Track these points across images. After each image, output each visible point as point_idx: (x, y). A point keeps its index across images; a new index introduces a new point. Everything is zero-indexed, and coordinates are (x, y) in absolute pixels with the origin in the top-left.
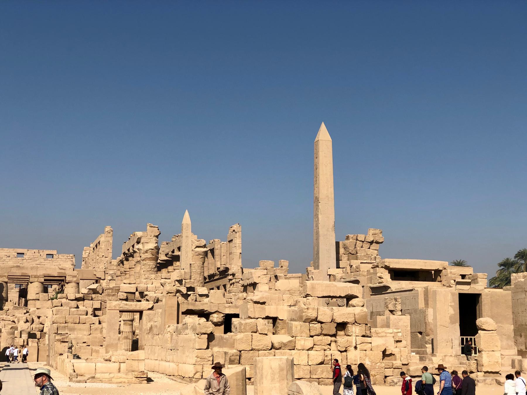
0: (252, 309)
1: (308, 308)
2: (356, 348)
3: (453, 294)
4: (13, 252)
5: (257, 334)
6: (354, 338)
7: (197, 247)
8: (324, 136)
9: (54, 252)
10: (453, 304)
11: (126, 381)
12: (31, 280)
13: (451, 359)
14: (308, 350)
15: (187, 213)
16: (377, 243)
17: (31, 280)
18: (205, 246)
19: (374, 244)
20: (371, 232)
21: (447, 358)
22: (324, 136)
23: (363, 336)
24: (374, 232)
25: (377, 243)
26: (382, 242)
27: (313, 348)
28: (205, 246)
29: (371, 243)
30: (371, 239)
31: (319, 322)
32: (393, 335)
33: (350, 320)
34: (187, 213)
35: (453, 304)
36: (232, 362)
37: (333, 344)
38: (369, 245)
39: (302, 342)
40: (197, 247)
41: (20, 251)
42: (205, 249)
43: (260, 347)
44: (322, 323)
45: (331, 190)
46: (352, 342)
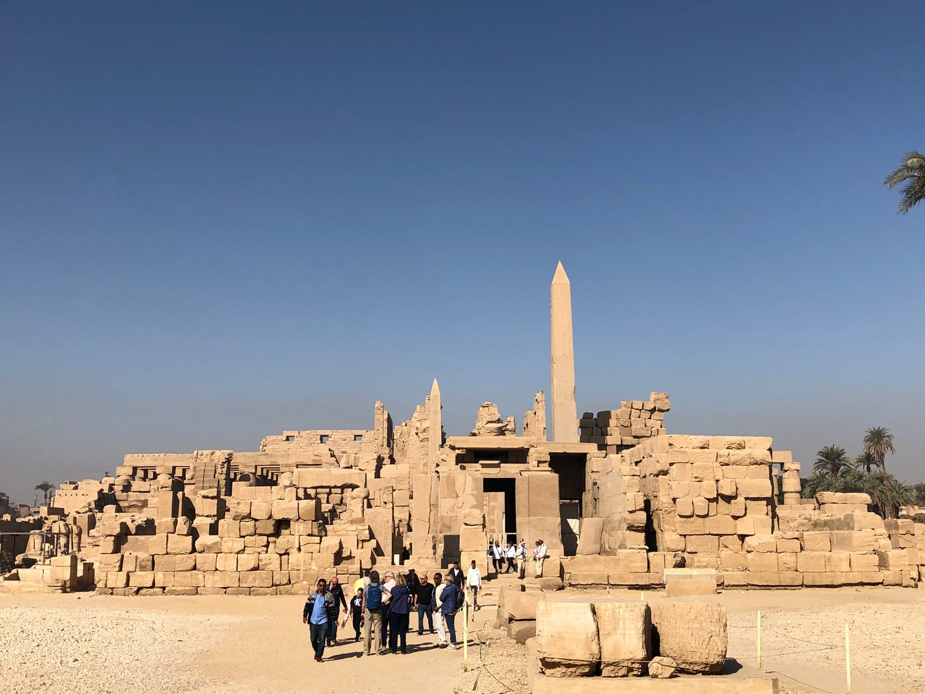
0: (200, 506)
1: (238, 503)
2: (299, 549)
3: (475, 480)
4: (350, 434)
5: (175, 535)
6: (297, 537)
7: (489, 422)
8: (561, 279)
9: (295, 433)
10: (475, 492)
11: (37, 589)
12: (282, 469)
13: (427, 562)
14: (238, 553)
15: (435, 383)
16: (661, 411)
17: (282, 469)
18: (499, 421)
19: (656, 412)
20: (653, 396)
21: (421, 561)
22: (561, 279)
23: (309, 535)
24: (656, 396)
25: (661, 411)
26: (668, 410)
27: (244, 550)
28: (499, 421)
29: (653, 411)
30: (650, 406)
31: (254, 519)
32: (356, 533)
33: (292, 515)
34: (435, 383)
35: (475, 492)
36: (143, 568)
37: (271, 546)
38: (648, 414)
39: (230, 544)
40: (489, 422)
41: (358, 432)
42: (500, 425)
43: (177, 551)
44: (256, 520)
45: (570, 347)
46: (294, 543)
